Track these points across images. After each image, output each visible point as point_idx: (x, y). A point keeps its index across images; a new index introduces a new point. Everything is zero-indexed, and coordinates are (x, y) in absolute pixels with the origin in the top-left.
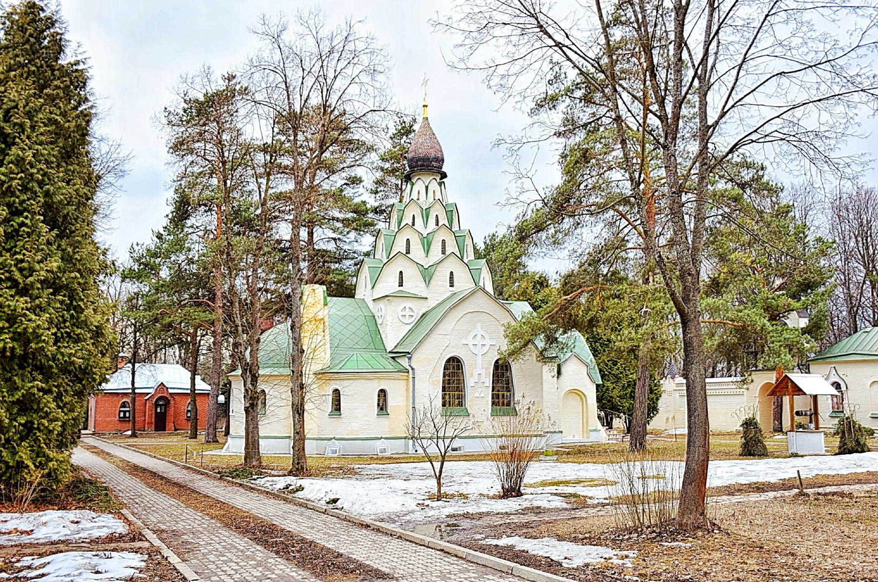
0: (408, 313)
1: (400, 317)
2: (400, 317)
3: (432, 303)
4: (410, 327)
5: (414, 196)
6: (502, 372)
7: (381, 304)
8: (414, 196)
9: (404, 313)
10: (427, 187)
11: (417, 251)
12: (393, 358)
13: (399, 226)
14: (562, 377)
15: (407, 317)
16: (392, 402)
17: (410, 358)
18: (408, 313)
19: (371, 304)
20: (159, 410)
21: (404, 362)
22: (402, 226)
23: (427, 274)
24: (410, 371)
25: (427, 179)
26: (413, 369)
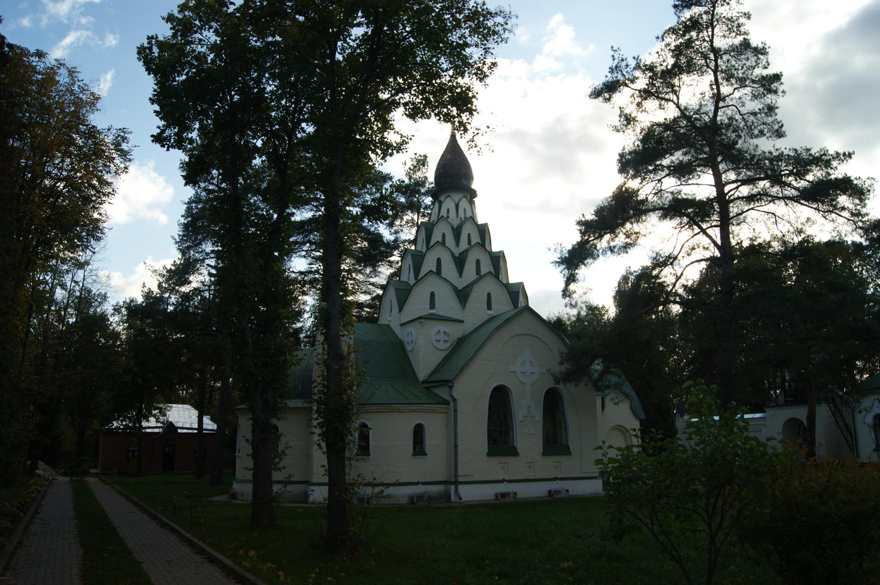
0: (442, 337)
1: (434, 342)
2: (434, 342)
3: (466, 328)
4: (444, 354)
5: (444, 213)
6: (552, 404)
7: (411, 329)
8: (444, 213)
9: (438, 338)
10: (457, 206)
11: (449, 269)
12: (427, 388)
13: (416, 274)
14: (606, 410)
15: (442, 342)
16: (431, 441)
17: (451, 387)
18: (442, 337)
19: (397, 330)
20: (167, 450)
21: (443, 392)
22: (420, 277)
23: (463, 295)
24: (452, 403)
25: (456, 197)
26: (454, 400)
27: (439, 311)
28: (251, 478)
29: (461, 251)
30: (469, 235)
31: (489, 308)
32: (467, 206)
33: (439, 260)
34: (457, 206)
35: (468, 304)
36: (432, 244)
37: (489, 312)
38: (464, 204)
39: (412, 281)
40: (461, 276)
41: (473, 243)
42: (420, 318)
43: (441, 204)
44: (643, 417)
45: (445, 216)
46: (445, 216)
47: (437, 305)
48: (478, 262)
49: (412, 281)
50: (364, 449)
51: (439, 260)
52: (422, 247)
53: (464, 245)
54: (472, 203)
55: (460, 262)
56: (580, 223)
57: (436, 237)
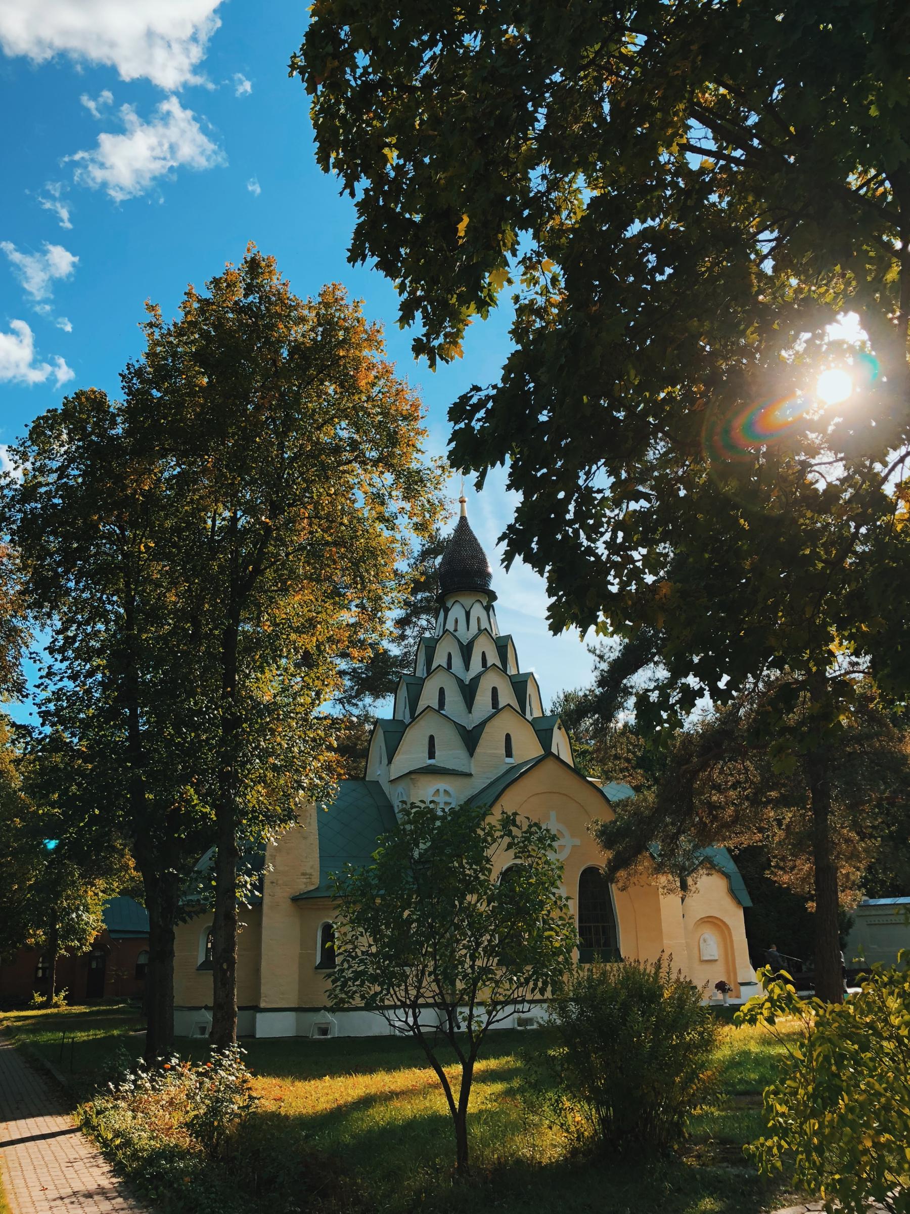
7: (400, 788)
8: (450, 626)
10: (468, 614)
11: (454, 702)
19: (386, 787)
20: (94, 965)
23: (471, 739)
25: (467, 601)
27: (442, 759)
28: (177, 1015)
29: (473, 675)
30: (484, 653)
31: (509, 754)
32: (483, 614)
33: (442, 691)
34: (468, 614)
35: (479, 750)
36: (433, 667)
37: (508, 760)
38: (477, 611)
39: (407, 720)
40: (470, 712)
41: (489, 665)
42: (410, 773)
43: (447, 611)
44: (749, 904)
45: (452, 629)
46: (452, 629)
47: (514, 752)
48: (495, 691)
49: (407, 720)
50: (708, 875)
51: (442, 691)
52: (421, 672)
53: (476, 665)
54: (489, 608)
55: (469, 691)
56: (556, 628)
57: (440, 659)
